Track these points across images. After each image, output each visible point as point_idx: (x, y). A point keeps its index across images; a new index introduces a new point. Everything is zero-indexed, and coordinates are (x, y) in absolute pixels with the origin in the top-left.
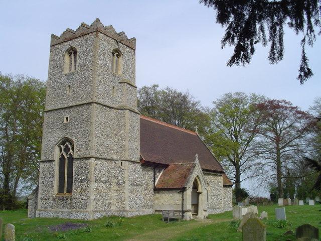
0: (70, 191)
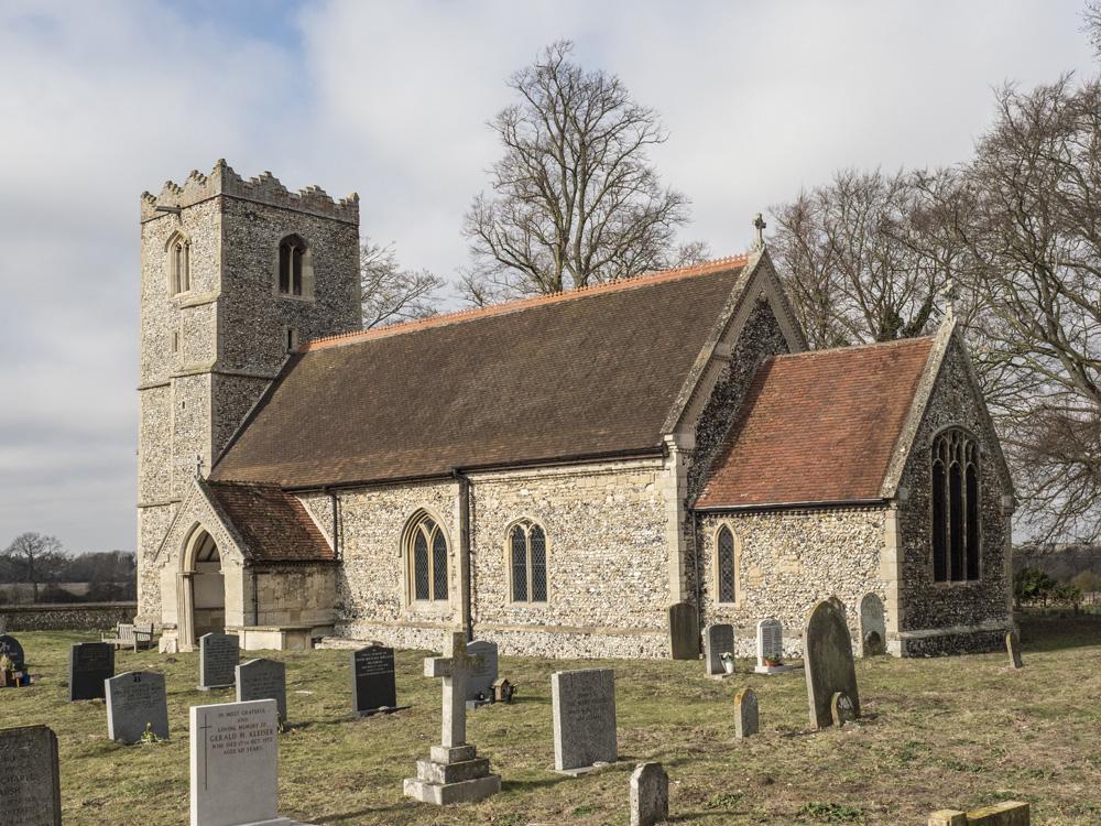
0: (540, 595)
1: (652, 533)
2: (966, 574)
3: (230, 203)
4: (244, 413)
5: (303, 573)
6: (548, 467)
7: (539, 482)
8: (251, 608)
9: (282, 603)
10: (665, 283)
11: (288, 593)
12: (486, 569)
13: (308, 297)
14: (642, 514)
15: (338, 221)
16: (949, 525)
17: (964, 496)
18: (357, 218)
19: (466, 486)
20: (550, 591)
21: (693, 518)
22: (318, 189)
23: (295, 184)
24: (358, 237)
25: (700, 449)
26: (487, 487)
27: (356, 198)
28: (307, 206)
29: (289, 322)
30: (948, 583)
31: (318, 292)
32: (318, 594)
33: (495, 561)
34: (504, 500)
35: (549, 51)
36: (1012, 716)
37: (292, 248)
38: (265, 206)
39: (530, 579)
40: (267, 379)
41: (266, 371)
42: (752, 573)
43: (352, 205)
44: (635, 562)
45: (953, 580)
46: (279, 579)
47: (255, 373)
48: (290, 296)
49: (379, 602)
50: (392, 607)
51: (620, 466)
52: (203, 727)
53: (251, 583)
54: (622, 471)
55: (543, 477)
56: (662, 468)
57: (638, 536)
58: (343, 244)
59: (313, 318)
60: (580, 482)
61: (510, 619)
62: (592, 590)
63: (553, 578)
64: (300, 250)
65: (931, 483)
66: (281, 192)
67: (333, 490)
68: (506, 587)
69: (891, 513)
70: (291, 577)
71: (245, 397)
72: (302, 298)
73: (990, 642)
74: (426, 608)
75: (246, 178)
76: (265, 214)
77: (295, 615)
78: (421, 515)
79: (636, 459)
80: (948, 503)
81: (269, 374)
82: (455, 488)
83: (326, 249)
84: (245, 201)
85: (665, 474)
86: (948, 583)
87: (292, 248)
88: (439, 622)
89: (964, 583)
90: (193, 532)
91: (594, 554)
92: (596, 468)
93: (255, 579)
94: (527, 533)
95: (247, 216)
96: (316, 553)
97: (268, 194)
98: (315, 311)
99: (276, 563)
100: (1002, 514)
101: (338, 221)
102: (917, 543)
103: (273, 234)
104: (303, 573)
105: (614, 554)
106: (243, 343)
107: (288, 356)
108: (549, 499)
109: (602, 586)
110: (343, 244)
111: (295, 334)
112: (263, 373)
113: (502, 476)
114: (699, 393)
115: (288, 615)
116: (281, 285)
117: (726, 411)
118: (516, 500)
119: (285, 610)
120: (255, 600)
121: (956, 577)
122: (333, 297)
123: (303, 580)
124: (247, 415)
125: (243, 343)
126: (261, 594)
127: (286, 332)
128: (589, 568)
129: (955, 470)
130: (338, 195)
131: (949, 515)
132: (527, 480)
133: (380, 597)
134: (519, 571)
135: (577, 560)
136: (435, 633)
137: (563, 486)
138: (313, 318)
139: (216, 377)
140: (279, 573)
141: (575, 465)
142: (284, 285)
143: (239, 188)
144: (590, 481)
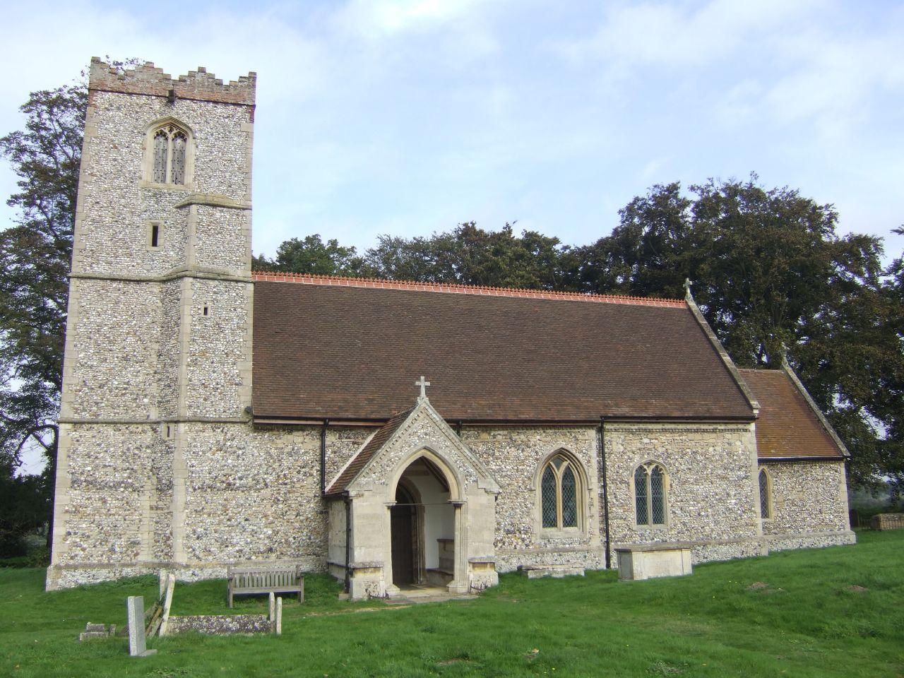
0: (659, 519)
1: (742, 473)
6: (671, 423)
7: (659, 434)
10: (254, 360)
12: (614, 501)
14: (735, 460)
19: (601, 430)
20: (669, 516)
26: (614, 435)
33: (625, 495)
34: (629, 448)
35: (827, 207)
39: (650, 506)
42: (779, 500)
44: (732, 493)
49: (508, 532)
50: (523, 536)
51: (723, 427)
54: (723, 430)
55: (665, 431)
56: (746, 430)
57: (732, 476)
60: (691, 436)
61: (637, 539)
62: (703, 514)
63: (672, 506)
67: (599, 424)
68: (633, 516)
69: (843, 464)
74: (560, 534)
75: (610, 235)
78: (562, 454)
79: (659, 423)
82: (592, 434)
85: (748, 435)
88: (576, 546)
90: (440, 459)
91: (701, 489)
92: (673, 426)
94: (649, 471)
105: (719, 488)
108: (667, 447)
109: (709, 510)
113: (633, 427)
114: (123, 421)
118: (639, 445)
128: (700, 498)
132: (650, 431)
133: (509, 527)
134: (641, 502)
135: (691, 492)
136: (578, 555)
137: (678, 438)
141: (691, 423)
144: (698, 436)
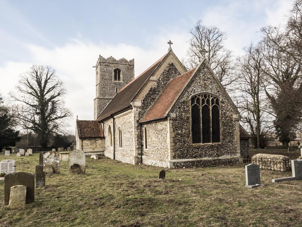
2: (211, 140)
3: (102, 63)
4: (105, 106)
5: (96, 140)
8: (81, 148)
9: (90, 146)
11: (91, 144)
13: (121, 81)
15: (129, 65)
16: (201, 125)
17: (211, 115)
18: (134, 64)
21: (140, 125)
22: (123, 58)
23: (118, 58)
24: (134, 68)
25: (144, 106)
27: (133, 59)
28: (121, 62)
29: (116, 87)
30: (201, 144)
31: (124, 80)
32: (100, 145)
36: (121, 192)
37: (117, 72)
38: (110, 63)
40: (111, 99)
41: (110, 97)
43: (132, 61)
45: (203, 142)
46: (89, 141)
47: (108, 98)
48: (117, 81)
52: (248, 170)
53: (81, 142)
58: (130, 69)
59: (122, 86)
64: (119, 71)
65: (190, 112)
66: (114, 60)
70: (92, 141)
71: (105, 103)
72: (120, 82)
73: (224, 163)
75: (106, 58)
76: (110, 65)
77: (93, 149)
80: (201, 118)
81: (111, 98)
83: (126, 71)
84: (105, 63)
86: (201, 143)
87: (117, 72)
89: (201, 144)
93: (82, 141)
95: (106, 66)
96: (99, 135)
97: (111, 61)
98: (123, 84)
99: (88, 138)
100: (234, 121)
101: (129, 65)
102: (182, 131)
103: (112, 69)
104: (96, 140)
106: (105, 92)
107: (116, 94)
110: (130, 69)
111: (118, 89)
112: (110, 98)
115: (92, 149)
116: (115, 78)
117: (155, 95)
119: (91, 148)
120: (82, 146)
121: (206, 140)
122: (128, 81)
123: (96, 141)
124: (106, 107)
125: (105, 92)
126: (84, 145)
127: (116, 89)
129: (206, 109)
130: (128, 59)
131: (201, 122)
138: (122, 86)
139: (98, 99)
140: (89, 140)
142: (115, 79)
143: (104, 60)
